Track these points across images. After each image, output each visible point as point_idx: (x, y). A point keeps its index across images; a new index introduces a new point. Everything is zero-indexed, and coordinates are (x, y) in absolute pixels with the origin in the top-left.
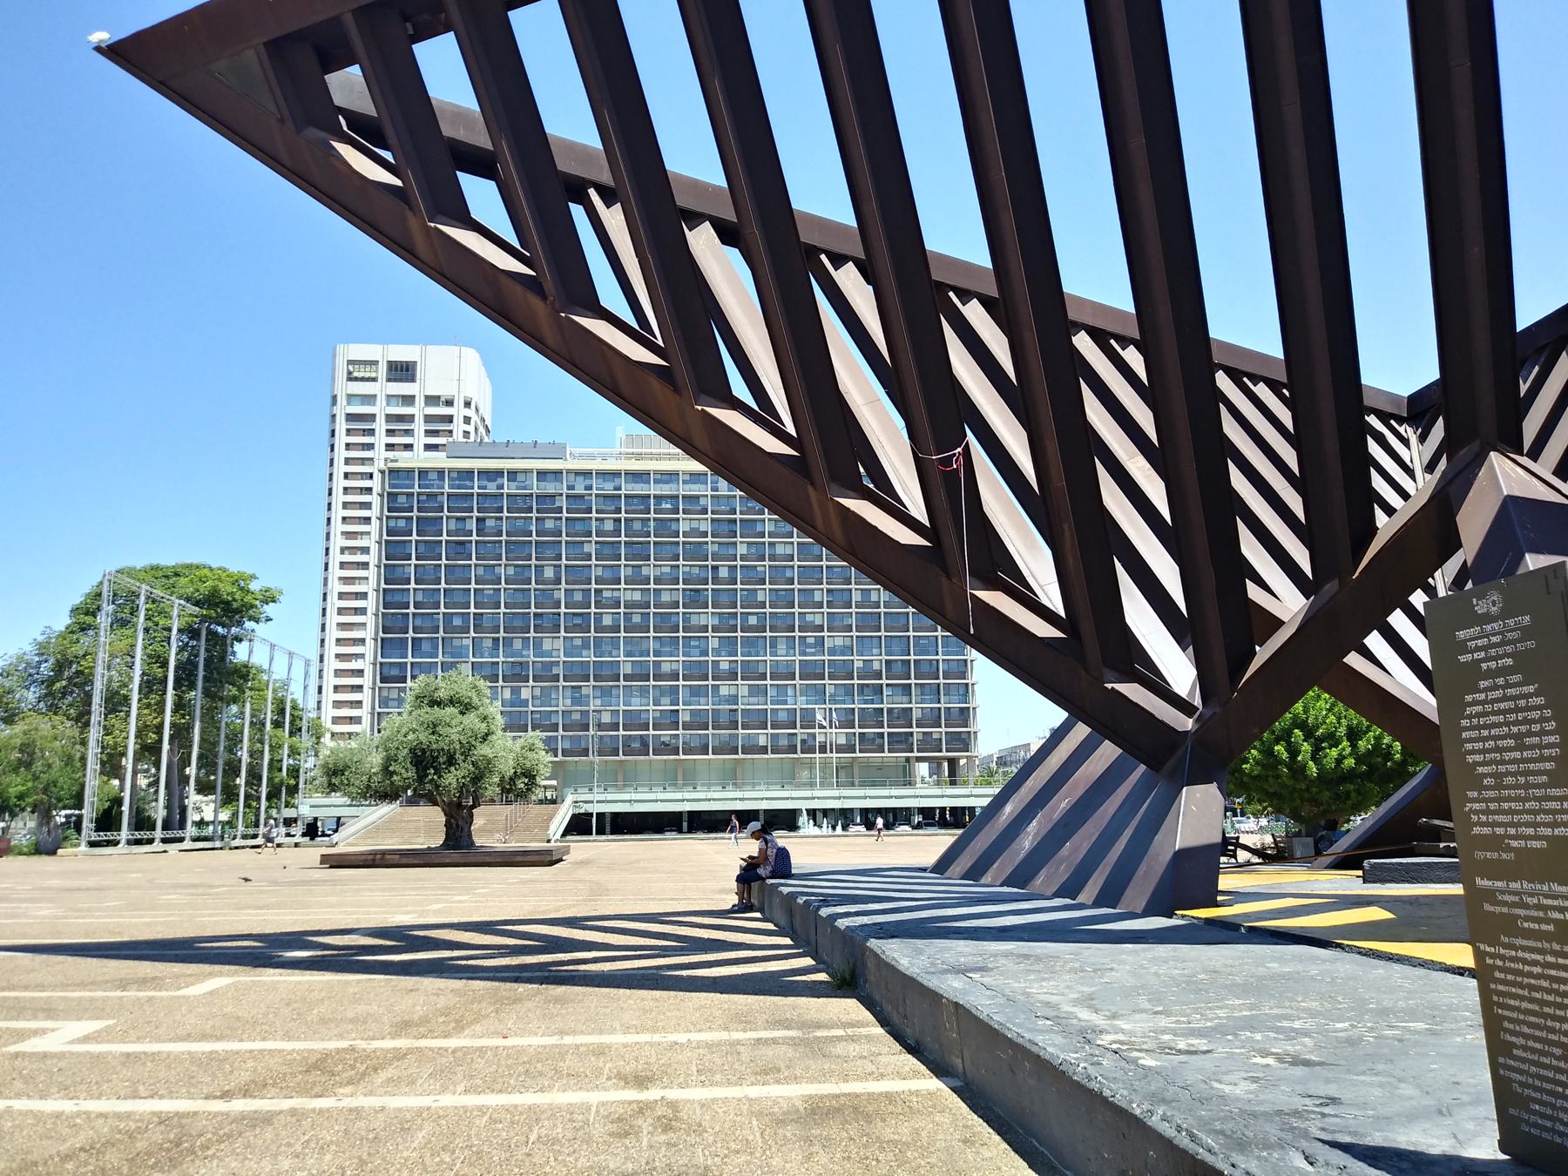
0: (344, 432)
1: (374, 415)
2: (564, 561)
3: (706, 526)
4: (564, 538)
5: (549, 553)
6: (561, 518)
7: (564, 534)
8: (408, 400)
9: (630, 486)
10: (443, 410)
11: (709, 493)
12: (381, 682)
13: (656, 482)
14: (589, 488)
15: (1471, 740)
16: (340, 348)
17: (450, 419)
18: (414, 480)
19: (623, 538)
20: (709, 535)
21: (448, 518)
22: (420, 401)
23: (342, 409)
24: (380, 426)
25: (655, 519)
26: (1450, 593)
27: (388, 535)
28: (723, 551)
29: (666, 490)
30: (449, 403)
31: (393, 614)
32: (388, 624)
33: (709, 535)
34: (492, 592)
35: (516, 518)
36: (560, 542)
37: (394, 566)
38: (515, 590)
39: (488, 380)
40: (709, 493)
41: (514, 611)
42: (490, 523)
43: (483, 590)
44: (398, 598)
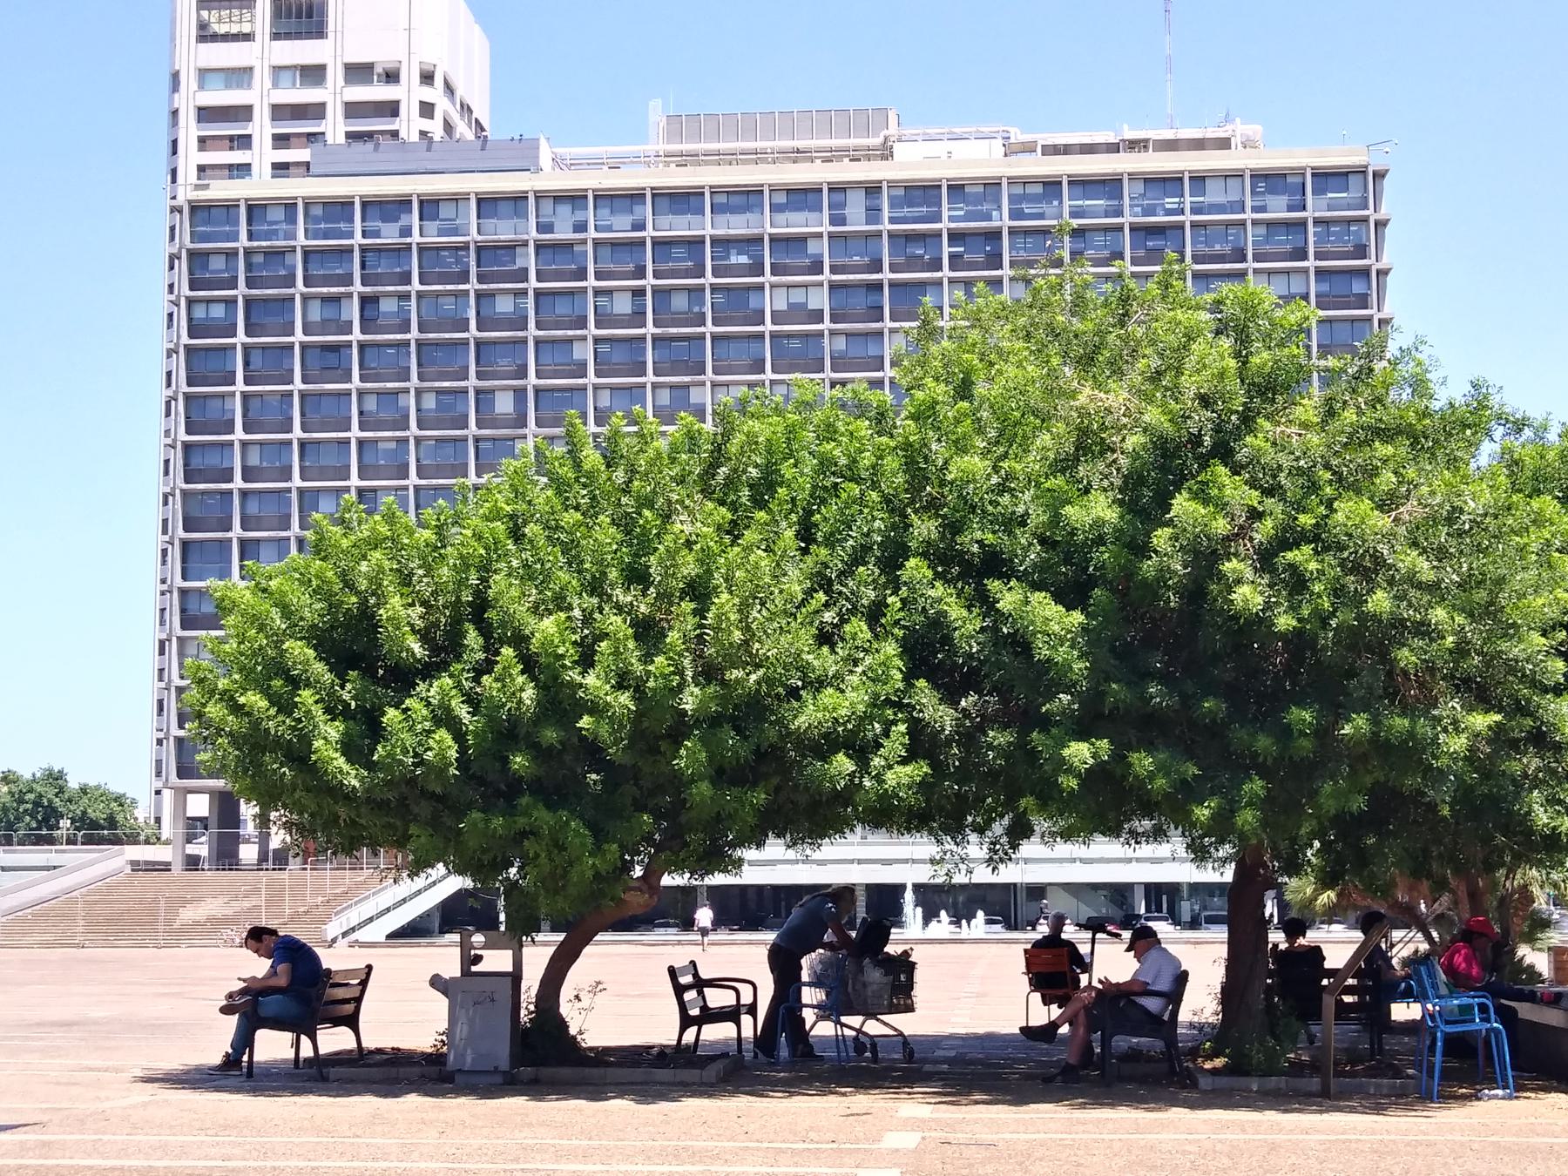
0: (194, 144)
1: (323, 105)
2: (532, 380)
3: (820, 300)
4: (532, 331)
5: (505, 364)
6: (524, 292)
7: (532, 324)
8: (313, 74)
9: (665, 220)
10: (378, 92)
11: (826, 228)
12: (183, 627)
13: (775, 208)
14: (581, 227)
17: (392, 109)
18: (237, 223)
19: (650, 329)
20: (827, 317)
21: (306, 298)
22: (335, 75)
23: (190, 98)
24: (262, 128)
25: (715, 289)
26: (1270, 946)
27: (191, 336)
28: (857, 351)
29: (736, 226)
30: (391, 77)
31: (204, 493)
32: (196, 513)
33: (827, 317)
34: (393, 445)
35: (438, 294)
36: (524, 341)
37: (206, 396)
38: (439, 440)
39: (477, 28)
40: (826, 228)
41: (434, 482)
42: (388, 306)
43: (376, 441)
44: (212, 460)
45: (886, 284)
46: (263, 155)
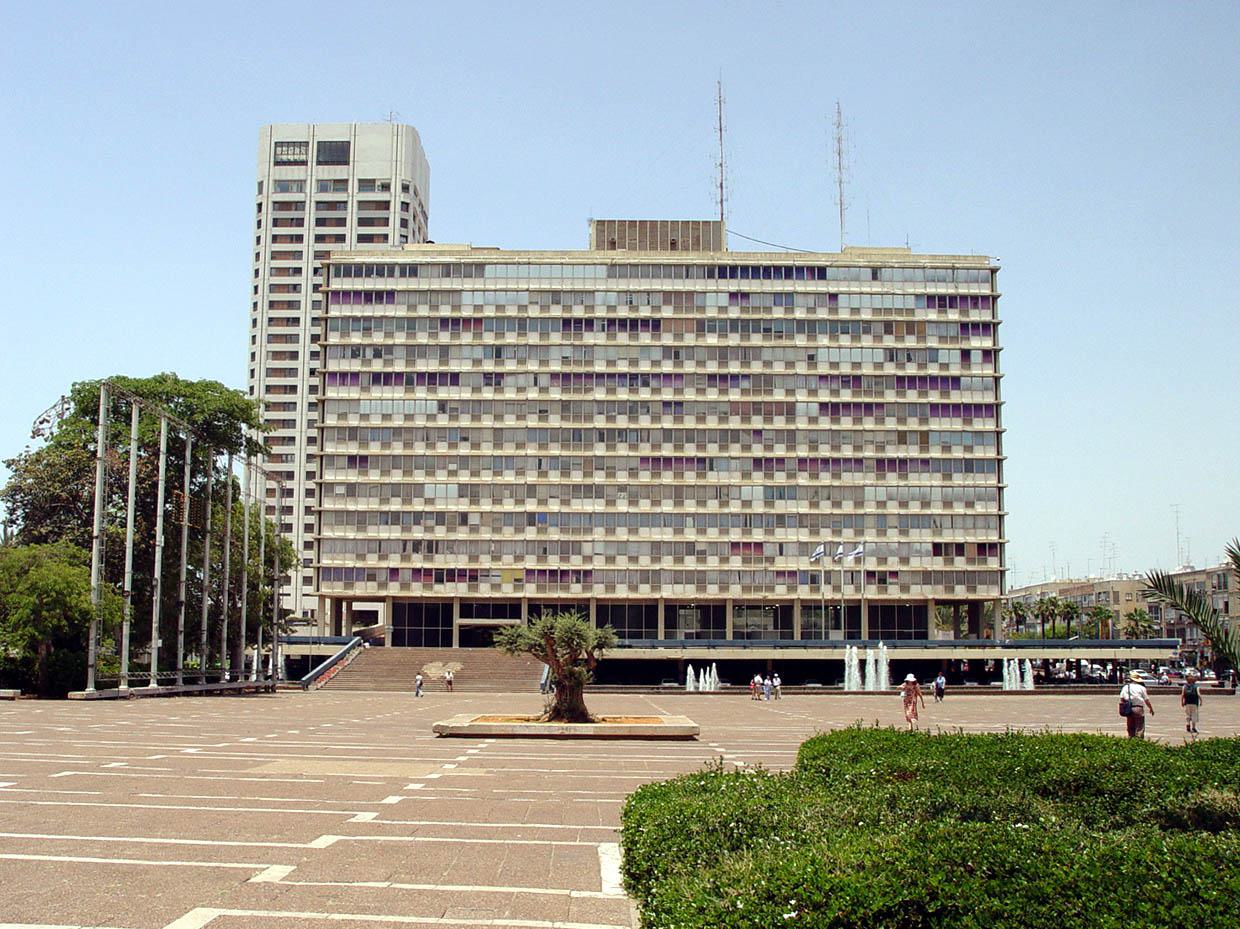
8: (341, 184)
22: (353, 186)
30: (386, 187)
46: (352, 230)
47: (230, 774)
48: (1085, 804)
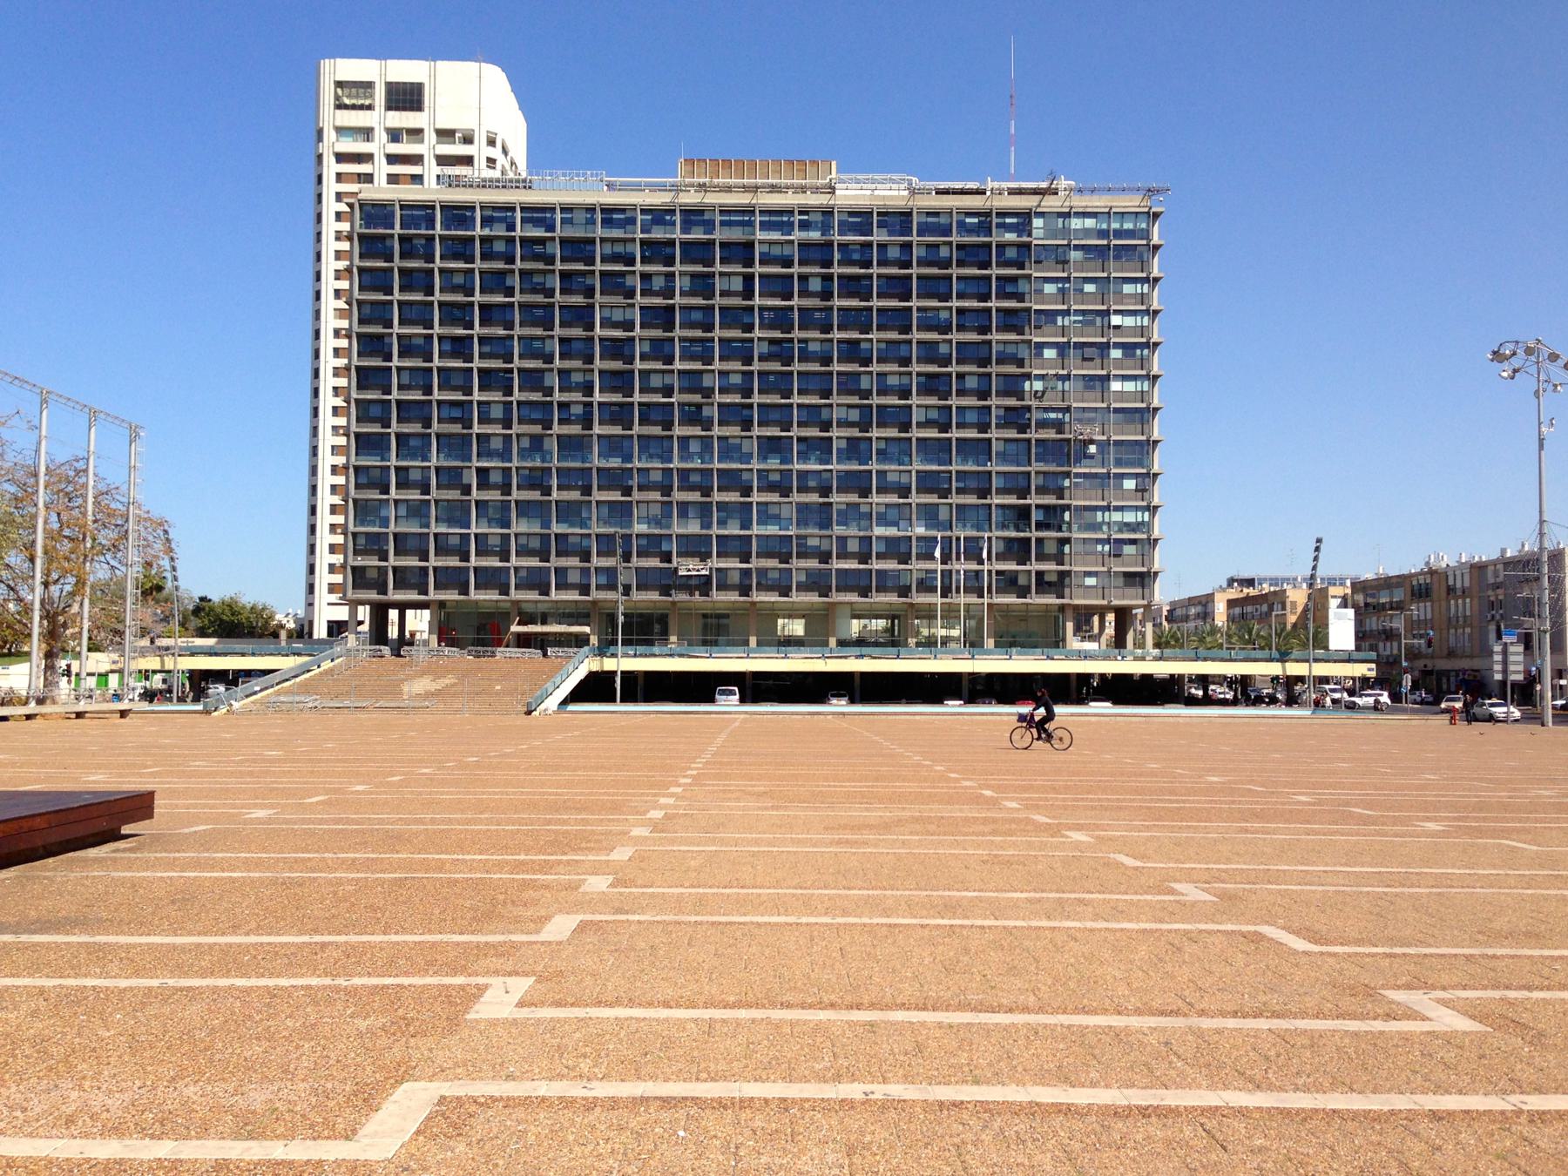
8: (416, 133)
15: (1464, 603)
16: (327, 65)
22: (429, 136)
45: (875, 276)
47: (246, 861)
48: (1061, 1046)
